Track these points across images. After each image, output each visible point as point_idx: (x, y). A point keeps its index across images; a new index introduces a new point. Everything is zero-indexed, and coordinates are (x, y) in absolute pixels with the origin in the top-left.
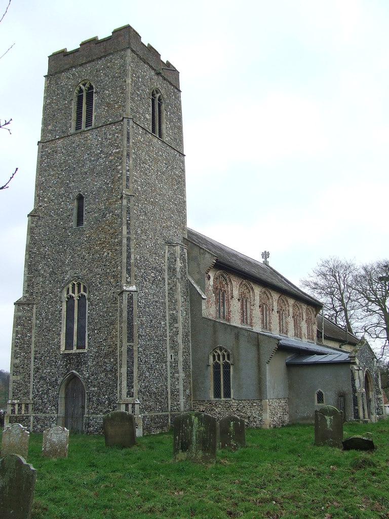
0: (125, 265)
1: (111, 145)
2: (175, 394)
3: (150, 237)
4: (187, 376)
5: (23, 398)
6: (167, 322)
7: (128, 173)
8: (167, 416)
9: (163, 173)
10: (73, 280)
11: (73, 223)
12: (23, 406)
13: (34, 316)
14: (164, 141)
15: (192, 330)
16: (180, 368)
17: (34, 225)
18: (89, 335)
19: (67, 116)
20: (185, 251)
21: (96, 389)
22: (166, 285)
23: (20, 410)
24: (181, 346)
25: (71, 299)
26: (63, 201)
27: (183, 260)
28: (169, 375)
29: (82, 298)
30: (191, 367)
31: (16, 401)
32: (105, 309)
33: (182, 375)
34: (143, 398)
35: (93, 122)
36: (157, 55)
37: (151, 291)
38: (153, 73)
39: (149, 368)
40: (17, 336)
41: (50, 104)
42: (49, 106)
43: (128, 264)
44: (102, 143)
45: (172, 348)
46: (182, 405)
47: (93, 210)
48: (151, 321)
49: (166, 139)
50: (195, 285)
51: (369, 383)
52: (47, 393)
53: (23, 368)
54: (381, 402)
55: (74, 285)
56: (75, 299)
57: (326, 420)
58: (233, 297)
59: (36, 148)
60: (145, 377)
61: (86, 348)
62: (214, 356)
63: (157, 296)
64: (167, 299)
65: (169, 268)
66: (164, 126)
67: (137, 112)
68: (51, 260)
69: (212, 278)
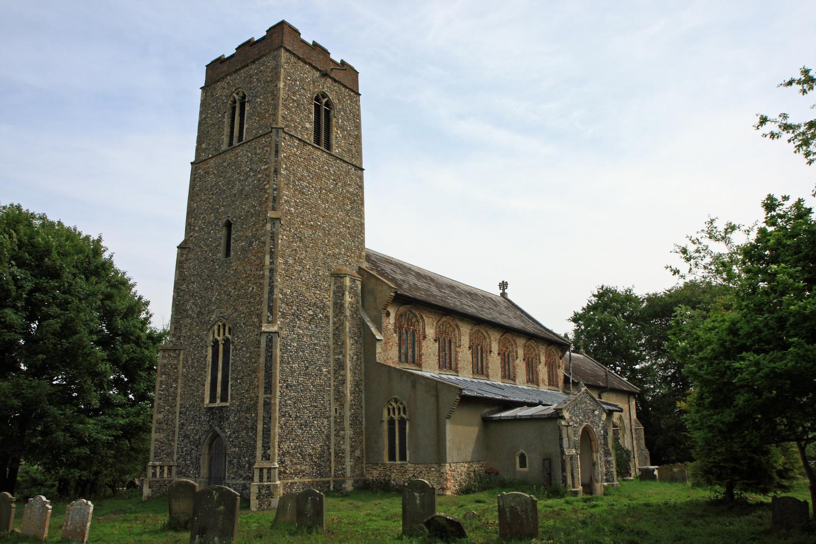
0: (265, 302)
1: (261, 161)
2: (340, 456)
3: (308, 267)
4: (357, 433)
5: (165, 459)
6: (331, 368)
7: (276, 192)
8: (329, 482)
9: (330, 191)
10: (218, 321)
11: (220, 255)
12: (166, 469)
13: (181, 363)
14: (333, 153)
15: (365, 378)
16: (347, 423)
17: (183, 259)
18: (232, 385)
19: (220, 131)
20: (359, 283)
21: (237, 449)
22: (331, 324)
23: (162, 473)
24: (349, 397)
25: (216, 343)
26: (213, 230)
27: (354, 294)
28: (333, 432)
29: (227, 342)
30: (364, 423)
31: (157, 463)
32: (248, 355)
33: (349, 432)
34: (291, 461)
35: (244, 137)
36: (326, 53)
37: (307, 332)
38: (317, 74)
39: (301, 425)
40: (161, 387)
41: (205, 118)
42: (204, 122)
43: (271, 299)
44: (251, 160)
45: (336, 400)
46: (348, 470)
47: (240, 237)
48: (307, 368)
49: (336, 151)
50: (370, 324)
51: (593, 442)
52: (190, 454)
53: (167, 424)
54: (611, 466)
55: (219, 326)
56: (220, 343)
57: (415, 498)
58: (426, 338)
59: (189, 168)
60: (296, 435)
61: (229, 401)
62: (389, 410)
63: (317, 338)
64: (331, 342)
65: (335, 304)
66: (333, 137)
67: (293, 120)
68: (199, 298)
69: (392, 315)
